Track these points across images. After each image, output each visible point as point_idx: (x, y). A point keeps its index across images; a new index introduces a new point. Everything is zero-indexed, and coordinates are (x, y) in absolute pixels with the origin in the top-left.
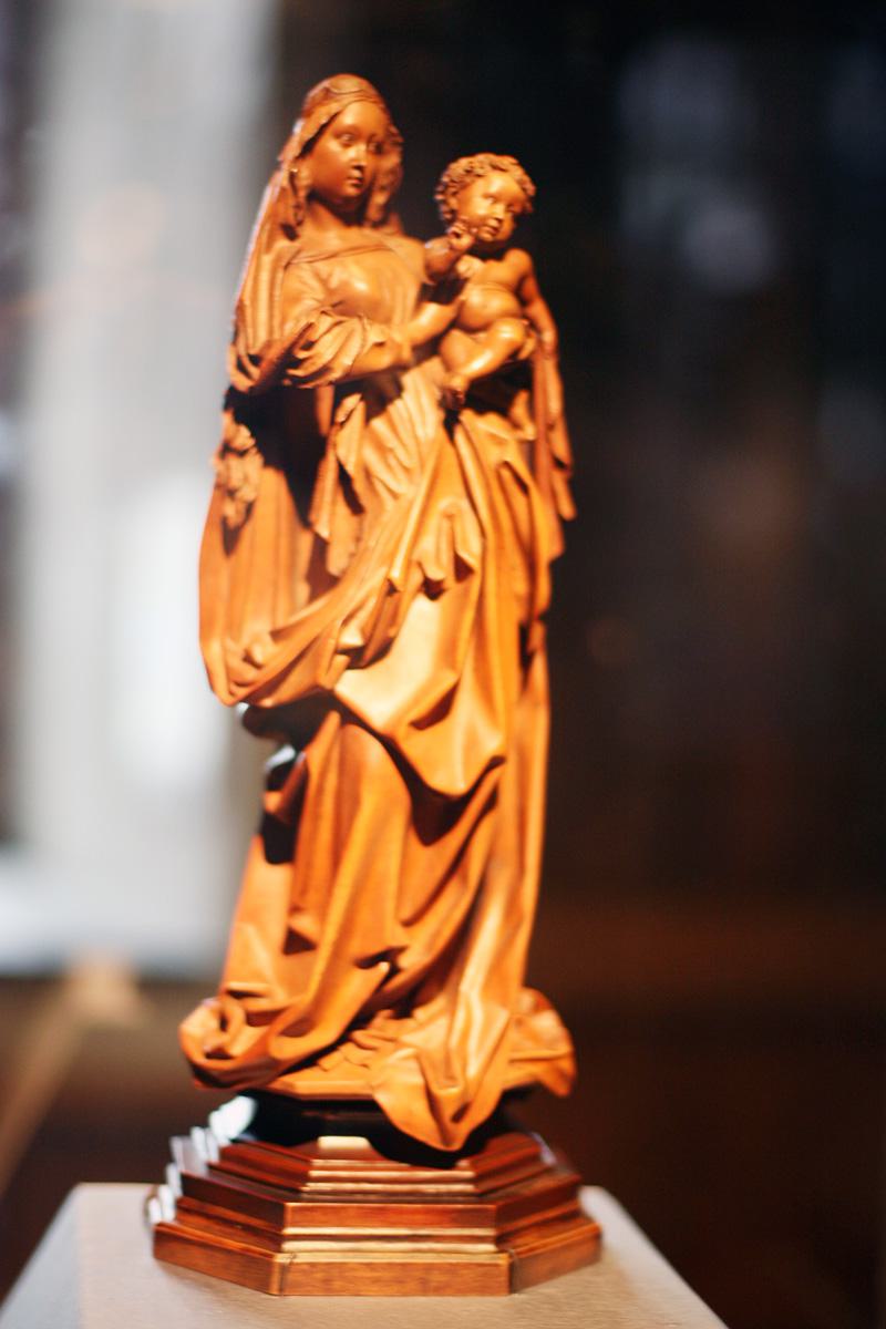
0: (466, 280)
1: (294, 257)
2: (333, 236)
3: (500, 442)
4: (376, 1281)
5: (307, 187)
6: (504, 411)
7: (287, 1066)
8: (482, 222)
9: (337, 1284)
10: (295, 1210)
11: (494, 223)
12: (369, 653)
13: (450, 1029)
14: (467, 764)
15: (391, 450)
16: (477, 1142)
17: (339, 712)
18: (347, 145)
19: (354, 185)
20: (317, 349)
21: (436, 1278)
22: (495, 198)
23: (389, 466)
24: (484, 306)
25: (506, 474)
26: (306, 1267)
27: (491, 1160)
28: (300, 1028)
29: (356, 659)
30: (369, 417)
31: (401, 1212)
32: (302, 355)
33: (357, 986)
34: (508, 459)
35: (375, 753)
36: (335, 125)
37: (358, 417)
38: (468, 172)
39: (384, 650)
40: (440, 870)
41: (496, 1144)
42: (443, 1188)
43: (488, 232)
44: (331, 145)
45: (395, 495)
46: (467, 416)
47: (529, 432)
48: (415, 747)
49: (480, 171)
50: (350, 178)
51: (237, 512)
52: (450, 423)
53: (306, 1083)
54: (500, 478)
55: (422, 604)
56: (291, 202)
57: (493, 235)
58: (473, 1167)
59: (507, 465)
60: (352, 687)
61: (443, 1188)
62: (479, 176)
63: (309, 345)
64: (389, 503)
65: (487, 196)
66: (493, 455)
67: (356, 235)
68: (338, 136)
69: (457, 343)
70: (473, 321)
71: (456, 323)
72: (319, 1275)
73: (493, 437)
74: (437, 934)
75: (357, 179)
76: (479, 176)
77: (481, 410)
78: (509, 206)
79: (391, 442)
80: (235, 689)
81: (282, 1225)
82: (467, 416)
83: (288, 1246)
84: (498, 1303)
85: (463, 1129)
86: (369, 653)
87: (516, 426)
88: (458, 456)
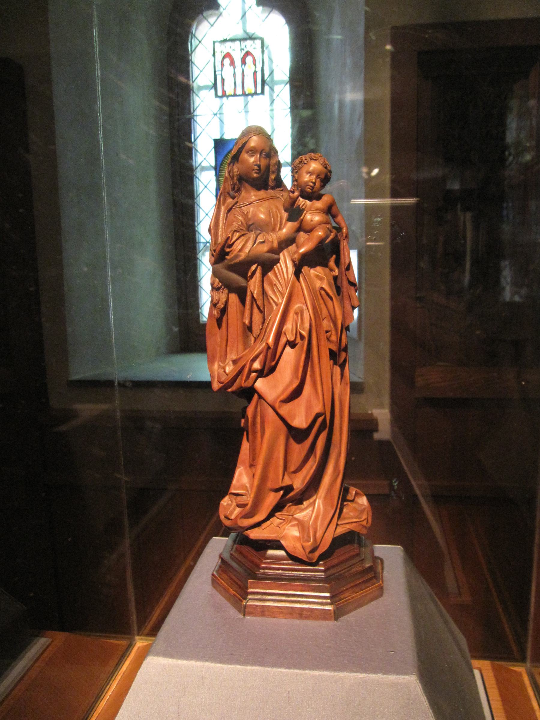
0: (303, 210)
1: (233, 206)
2: (253, 195)
3: (321, 279)
4: (282, 613)
5: (237, 175)
6: (325, 264)
7: (246, 528)
8: (306, 183)
9: (267, 613)
10: (251, 582)
11: (311, 184)
12: (266, 371)
13: (313, 511)
14: (307, 417)
15: (275, 285)
16: (322, 557)
18: (252, 156)
19: (256, 173)
20: (234, 247)
21: (305, 613)
22: (311, 174)
23: (274, 292)
24: (311, 221)
25: (323, 292)
26: (254, 607)
27: (334, 560)
28: (250, 515)
29: (261, 373)
30: (264, 274)
31: (292, 585)
32: (228, 250)
33: (272, 499)
34: (323, 286)
36: (247, 147)
37: (258, 274)
38: (301, 162)
39: (272, 370)
40: (303, 454)
41: (338, 552)
43: (309, 189)
44: (244, 156)
45: (277, 304)
46: (305, 269)
47: (336, 272)
48: (284, 410)
49: (305, 161)
50: (254, 170)
51: (217, 313)
52: (297, 273)
53: (255, 534)
54: (320, 294)
55: (288, 349)
57: (312, 190)
58: (324, 565)
59: (322, 288)
60: (260, 384)
62: (305, 164)
63: (231, 246)
64: (275, 307)
66: (318, 284)
67: (262, 193)
68: (247, 152)
69: (302, 236)
70: (308, 228)
71: (299, 229)
73: (317, 276)
74: (305, 477)
75: (257, 170)
76: (305, 164)
77: (312, 265)
79: (275, 281)
80: (219, 383)
82: (305, 269)
83: (250, 597)
85: (317, 554)
86: (266, 371)
87: (332, 270)
88: (301, 287)
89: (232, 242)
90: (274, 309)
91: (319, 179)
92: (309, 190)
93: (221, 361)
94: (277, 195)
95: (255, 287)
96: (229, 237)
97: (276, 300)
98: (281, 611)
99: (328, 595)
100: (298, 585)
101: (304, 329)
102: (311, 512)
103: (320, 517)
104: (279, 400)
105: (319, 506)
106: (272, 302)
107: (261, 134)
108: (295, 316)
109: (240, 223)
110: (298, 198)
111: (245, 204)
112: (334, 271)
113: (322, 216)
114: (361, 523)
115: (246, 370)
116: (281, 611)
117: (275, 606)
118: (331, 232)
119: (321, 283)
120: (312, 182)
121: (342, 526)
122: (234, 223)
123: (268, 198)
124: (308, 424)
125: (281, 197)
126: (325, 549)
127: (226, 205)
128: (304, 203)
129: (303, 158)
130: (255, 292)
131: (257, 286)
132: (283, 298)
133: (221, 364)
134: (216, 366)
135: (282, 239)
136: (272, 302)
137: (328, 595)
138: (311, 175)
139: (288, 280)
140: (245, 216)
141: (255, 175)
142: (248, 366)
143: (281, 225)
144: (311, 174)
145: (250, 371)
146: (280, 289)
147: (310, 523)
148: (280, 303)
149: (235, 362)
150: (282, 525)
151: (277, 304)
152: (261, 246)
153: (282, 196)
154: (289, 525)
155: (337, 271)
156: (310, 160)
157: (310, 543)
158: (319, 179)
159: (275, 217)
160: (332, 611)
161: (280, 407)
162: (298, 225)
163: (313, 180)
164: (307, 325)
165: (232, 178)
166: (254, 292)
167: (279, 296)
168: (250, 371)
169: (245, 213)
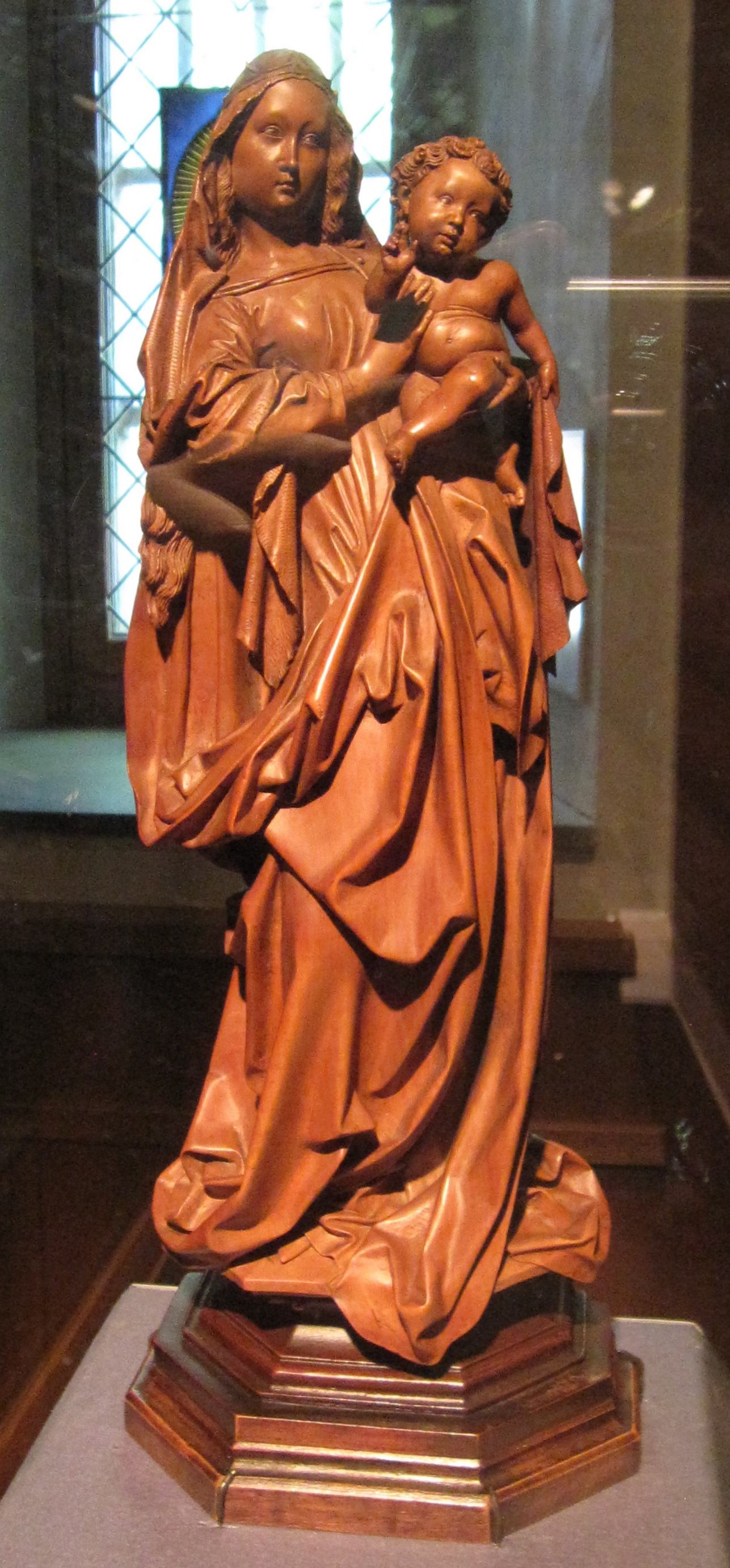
1: (214, 290)
3: (473, 515)
4: (335, 1515)
5: (228, 199)
6: (486, 472)
7: (232, 1259)
8: (435, 228)
9: (289, 1516)
10: (243, 1422)
11: (449, 229)
13: (434, 1212)
15: (335, 530)
17: (275, 857)
18: (275, 141)
19: (285, 192)
20: (214, 414)
21: (404, 1517)
22: (451, 198)
23: (332, 552)
25: (478, 555)
26: (252, 1495)
27: (494, 1360)
30: (303, 497)
32: (195, 422)
34: (480, 537)
35: (313, 907)
36: (258, 114)
37: (285, 497)
39: (322, 784)
40: (409, 1040)
41: (507, 1336)
42: (353, 1492)
44: (251, 140)
45: (338, 589)
46: (426, 485)
47: (520, 495)
49: (433, 161)
50: (278, 183)
51: (160, 610)
55: (370, 723)
56: (206, 218)
57: (451, 246)
59: (476, 544)
61: (353, 1492)
62: (432, 168)
63: (203, 410)
64: (332, 597)
65: (440, 195)
66: (464, 530)
67: (301, 254)
68: (261, 130)
69: (420, 385)
71: (410, 365)
72: (266, 1505)
74: (414, 1109)
76: (432, 168)
77: (448, 474)
78: (470, 206)
81: (231, 1440)
82: (426, 485)
84: (483, 1550)
89: (208, 399)
90: (331, 602)
91: (474, 215)
92: (443, 246)
93: (168, 756)
94: (348, 260)
95: (273, 535)
96: (199, 384)
97: (336, 575)
98: (332, 1509)
99: (473, 1464)
100: (383, 1434)
101: (418, 666)
102: (427, 1216)
103: (456, 1231)
104: (338, 877)
105: (452, 1197)
106: (324, 580)
107: (302, 77)
108: (393, 625)
109: (235, 342)
110: (408, 269)
111: (249, 284)
112: (514, 493)
113: (481, 327)
114: (577, 1250)
115: (243, 784)
116: (332, 1509)
117: (314, 1496)
118: (507, 374)
119: (473, 528)
120: (451, 224)
121: (520, 1258)
122: (216, 343)
123: (320, 270)
124: (426, 950)
125: (358, 268)
126: (469, 1325)
127: (192, 286)
128: (426, 285)
129: (428, 152)
130: (275, 551)
131: (279, 533)
132: (358, 569)
133: (168, 766)
134: (152, 770)
135: (360, 392)
136: (324, 580)
137: (473, 1464)
138: (449, 203)
139: (373, 516)
140: (250, 321)
141: (282, 199)
142: (248, 771)
143: (356, 350)
144: (451, 198)
145: (255, 788)
146: (351, 543)
147: (426, 1248)
148: (348, 585)
149: (209, 759)
150: (339, 1252)
151: (338, 589)
152: (295, 412)
153: (362, 263)
154: (363, 1252)
155: (521, 492)
156: (447, 157)
157: (422, 1307)
158: (474, 215)
159: (340, 326)
160: (486, 1514)
161: (341, 896)
162: (409, 352)
163: (455, 216)
164: (428, 654)
165: (213, 206)
166: (271, 551)
167: (345, 563)
168: (255, 788)
169: (250, 313)
